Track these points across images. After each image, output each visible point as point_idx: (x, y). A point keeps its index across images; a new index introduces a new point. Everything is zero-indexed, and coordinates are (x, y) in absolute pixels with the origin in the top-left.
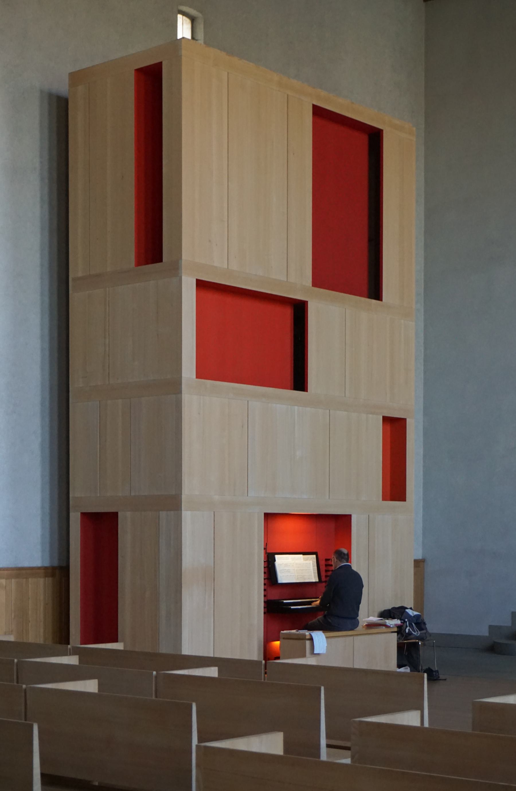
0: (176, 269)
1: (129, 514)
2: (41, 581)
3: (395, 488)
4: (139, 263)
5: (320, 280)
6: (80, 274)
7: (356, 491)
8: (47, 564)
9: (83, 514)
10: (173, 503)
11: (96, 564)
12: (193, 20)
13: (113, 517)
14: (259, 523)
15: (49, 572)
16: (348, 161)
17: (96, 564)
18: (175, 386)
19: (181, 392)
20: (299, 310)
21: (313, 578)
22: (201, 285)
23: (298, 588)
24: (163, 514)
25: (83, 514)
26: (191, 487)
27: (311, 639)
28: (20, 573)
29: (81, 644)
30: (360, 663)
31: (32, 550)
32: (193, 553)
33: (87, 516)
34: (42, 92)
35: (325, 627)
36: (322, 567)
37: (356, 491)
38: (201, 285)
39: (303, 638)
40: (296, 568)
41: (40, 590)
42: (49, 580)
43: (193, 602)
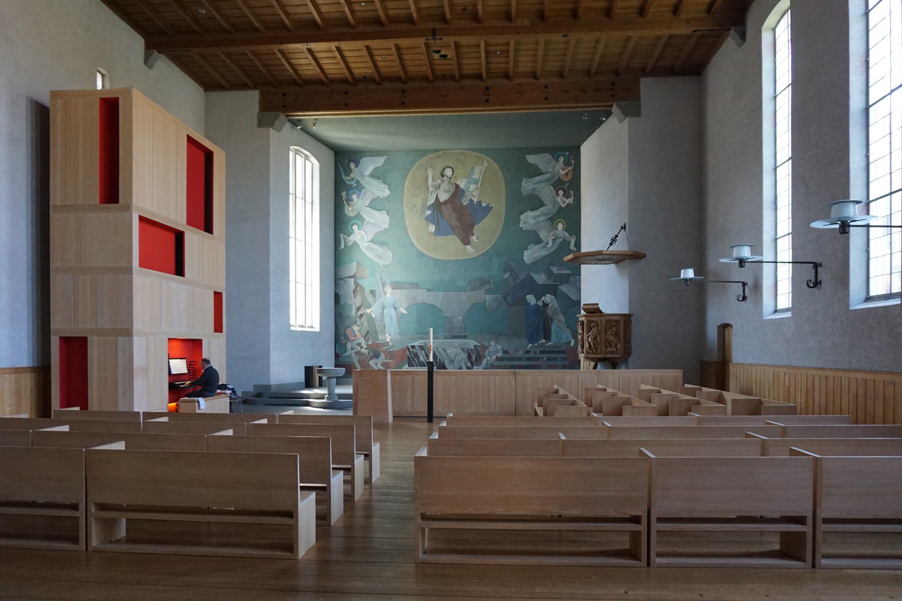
0: (128, 208)
1: (95, 338)
2: (29, 375)
3: (218, 328)
4: (101, 202)
5: (190, 222)
6: (58, 203)
7: (202, 329)
8: (31, 365)
9: (61, 338)
10: (128, 333)
11: (65, 366)
12: (103, 76)
13: (84, 340)
14: (166, 342)
15: (32, 370)
16: (201, 163)
17: (65, 366)
18: (129, 270)
19: (132, 273)
20: (179, 237)
21: (186, 371)
22: (142, 219)
23: (180, 376)
24: (120, 339)
25: (61, 338)
26: (137, 325)
27: (198, 402)
28: (17, 371)
29: (61, 407)
30: (216, 411)
31: (24, 357)
32: (138, 360)
33: (66, 341)
34: (27, 97)
35: (204, 396)
36: (189, 365)
37: (202, 329)
38: (142, 219)
39: (194, 401)
40: (179, 366)
41: (28, 382)
42: (33, 374)
43: (139, 384)
